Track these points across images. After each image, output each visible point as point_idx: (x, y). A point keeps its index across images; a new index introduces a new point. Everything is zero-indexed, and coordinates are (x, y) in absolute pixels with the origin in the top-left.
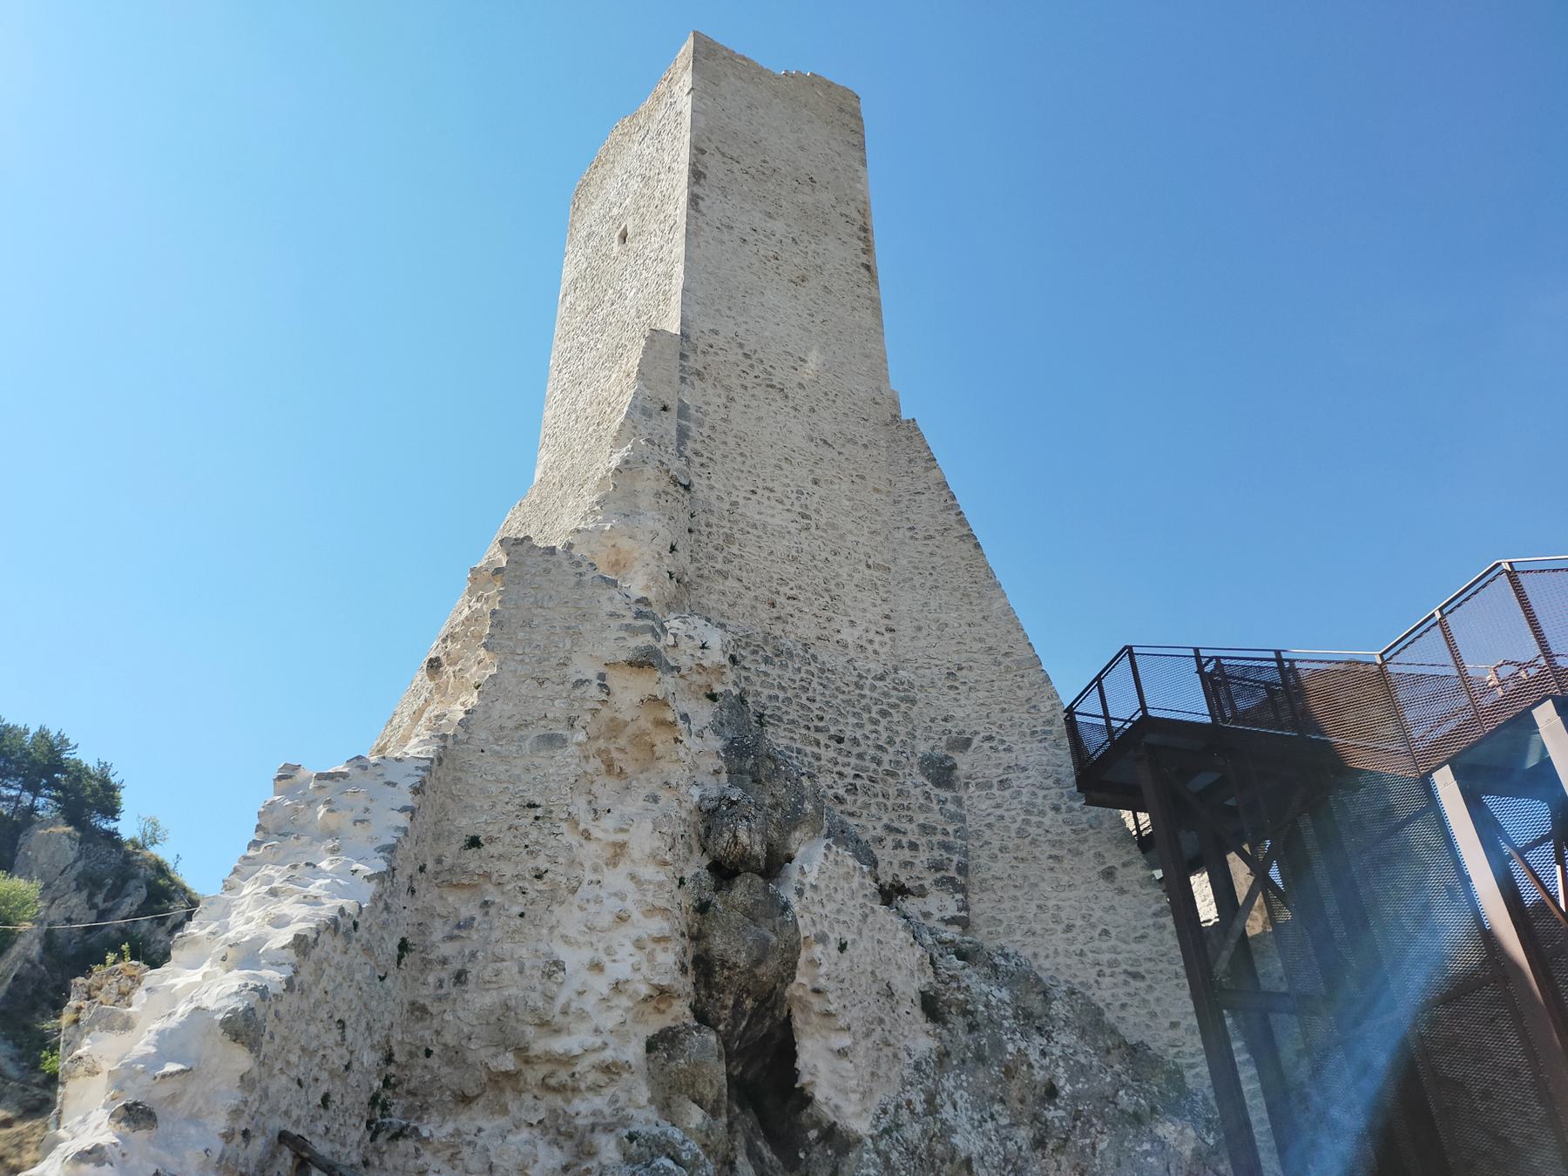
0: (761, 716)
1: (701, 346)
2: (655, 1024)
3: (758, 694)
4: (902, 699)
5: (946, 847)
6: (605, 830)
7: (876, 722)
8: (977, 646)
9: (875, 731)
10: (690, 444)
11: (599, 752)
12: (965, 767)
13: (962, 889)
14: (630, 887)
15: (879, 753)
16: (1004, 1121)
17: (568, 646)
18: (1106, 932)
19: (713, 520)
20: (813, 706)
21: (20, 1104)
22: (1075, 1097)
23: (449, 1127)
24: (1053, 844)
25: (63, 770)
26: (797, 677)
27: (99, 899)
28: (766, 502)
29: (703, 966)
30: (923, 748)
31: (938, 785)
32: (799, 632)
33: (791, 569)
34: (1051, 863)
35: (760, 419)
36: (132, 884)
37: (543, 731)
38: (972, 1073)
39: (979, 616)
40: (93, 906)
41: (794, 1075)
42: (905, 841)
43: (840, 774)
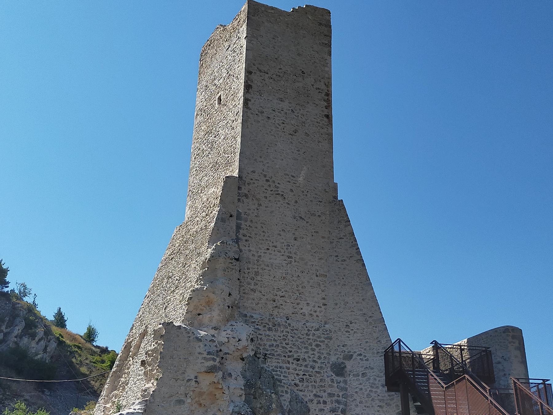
0: (266, 354)
3: (265, 345)
4: (326, 338)
5: (338, 402)
7: (313, 350)
9: (313, 354)
11: (196, 402)
12: (349, 367)
15: (314, 364)
17: (185, 366)
19: (250, 266)
20: (287, 347)
24: (380, 401)
26: (282, 335)
28: (273, 253)
30: (333, 359)
31: (337, 375)
32: (285, 312)
34: (378, 408)
36: (18, 319)
37: (177, 399)
39: (362, 298)
42: (321, 400)
43: (297, 374)
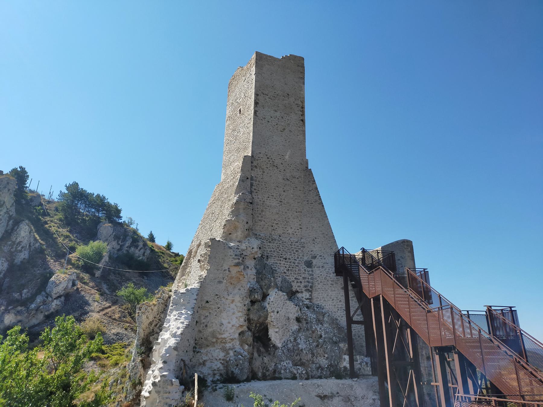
1: (257, 158)
2: (241, 330)
5: (308, 282)
6: (230, 298)
7: (294, 253)
8: (320, 232)
10: (253, 187)
13: (311, 291)
14: (235, 307)
16: (311, 341)
18: (340, 301)
19: (259, 207)
21: (112, 301)
22: (325, 338)
23: (206, 350)
24: (332, 281)
25: (105, 206)
27: (120, 242)
29: (249, 320)
30: (306, 258)
31: (308, 267)
33: (277, 216)
35: (271, 176)
36: (128, 237)
38: (305, 332)
40: (119, 244)
41: (268, 335)
